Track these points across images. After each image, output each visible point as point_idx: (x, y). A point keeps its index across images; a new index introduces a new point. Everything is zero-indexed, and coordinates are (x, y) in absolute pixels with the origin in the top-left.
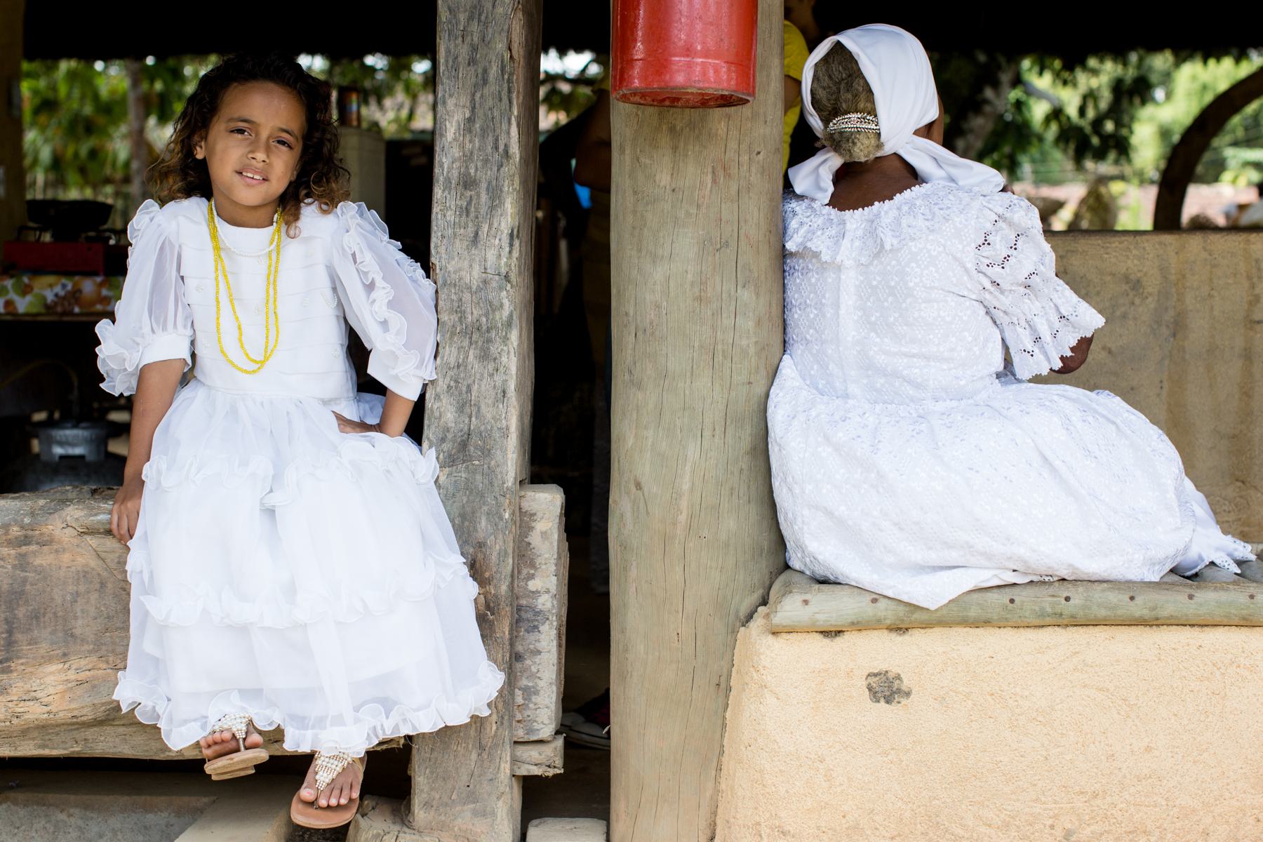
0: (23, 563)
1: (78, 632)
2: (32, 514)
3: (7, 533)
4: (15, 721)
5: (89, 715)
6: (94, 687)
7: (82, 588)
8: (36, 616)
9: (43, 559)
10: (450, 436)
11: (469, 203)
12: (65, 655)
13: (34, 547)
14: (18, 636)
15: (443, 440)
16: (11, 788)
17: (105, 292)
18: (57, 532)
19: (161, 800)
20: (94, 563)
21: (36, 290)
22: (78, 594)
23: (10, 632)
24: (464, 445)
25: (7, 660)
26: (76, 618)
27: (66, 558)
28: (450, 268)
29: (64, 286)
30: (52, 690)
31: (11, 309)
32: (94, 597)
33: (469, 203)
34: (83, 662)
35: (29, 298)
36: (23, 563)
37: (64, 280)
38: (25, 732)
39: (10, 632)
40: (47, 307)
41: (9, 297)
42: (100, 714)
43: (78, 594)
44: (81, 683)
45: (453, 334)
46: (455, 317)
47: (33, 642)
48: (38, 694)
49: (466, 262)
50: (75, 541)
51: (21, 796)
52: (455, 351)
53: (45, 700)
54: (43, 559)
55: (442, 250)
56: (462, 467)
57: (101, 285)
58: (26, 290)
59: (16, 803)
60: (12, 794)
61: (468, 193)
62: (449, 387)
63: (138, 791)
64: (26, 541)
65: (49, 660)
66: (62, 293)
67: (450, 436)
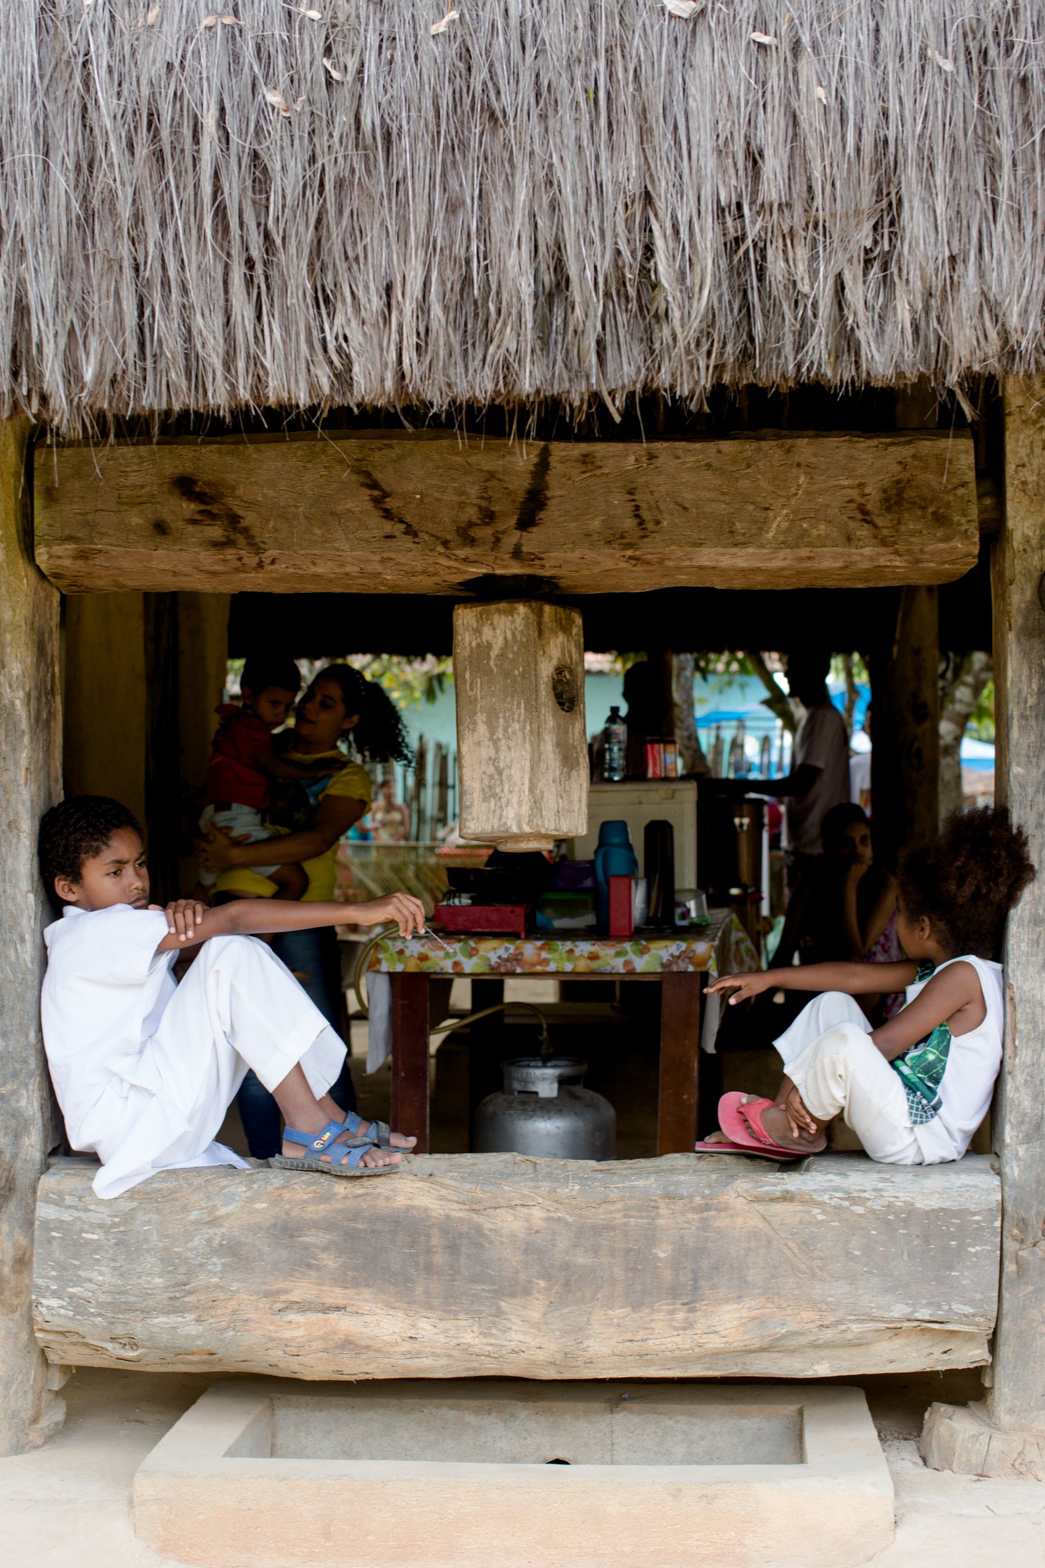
0: (705, 1225)
1: (750, 1279)
2: (709, 1186)
3: (691, 1202)
4: (697, 1350)
5: (757, 1344)
6: (763, 1322)
7: (753, 1245)
8: (716, 1268)
9: (721, 1222)
10: (1027, 1120)
11: (1039, 937)
12: (739, 1297)
13: (713, 1213)
14: (702, 1283)
15: (1022, 1122)
16: (625, 1400)
17: (544, 955)
18: (731, 1201)
19: (753, 1408)
20: (761, 1224)
21: (481, 953)
22: (749, 1249)
23: (695, 1280)
24: (1038, 1127)
25: (693, 1302)
26: (748, 1268)
27: (739, 1220)
28: (1025, 988)
29: (507, 949)
30: (728, 1325)
31: (458, 970)
32: (763, 1251)
33: (1039, 937)
34: (753, 1303)
35: (475, 959)
36: (705, 1225)
37: (507, 945)
38: (699, 1358)
39: (695, 1280)
40: (492, 968)
41: (456, 959)
42: (765, 1343)
43: (749, 1249)
44: (752, 1319)
45: (1028, 1040)
46: (1030, 1027)
47: (714, 1287)
48: (717, 1329)
49: (1037, 984)
50: (746, 1208)
51: (636, 1406)
52: (1030, 1052)
53: (724, 1333)
54: (721, 1222)
55: (1018, 973)
56: (1037, 1144)
57: (541, 948)
58: (472, 953)
59: (631, 1412)
60: (628, 1405)
61: (1038, 929)
62: (1026, 1081)
63: (731, 1401)
64: (707, 1208)
65: (727, 1301)
66: (505, 956)
67: (1027, 1120)
